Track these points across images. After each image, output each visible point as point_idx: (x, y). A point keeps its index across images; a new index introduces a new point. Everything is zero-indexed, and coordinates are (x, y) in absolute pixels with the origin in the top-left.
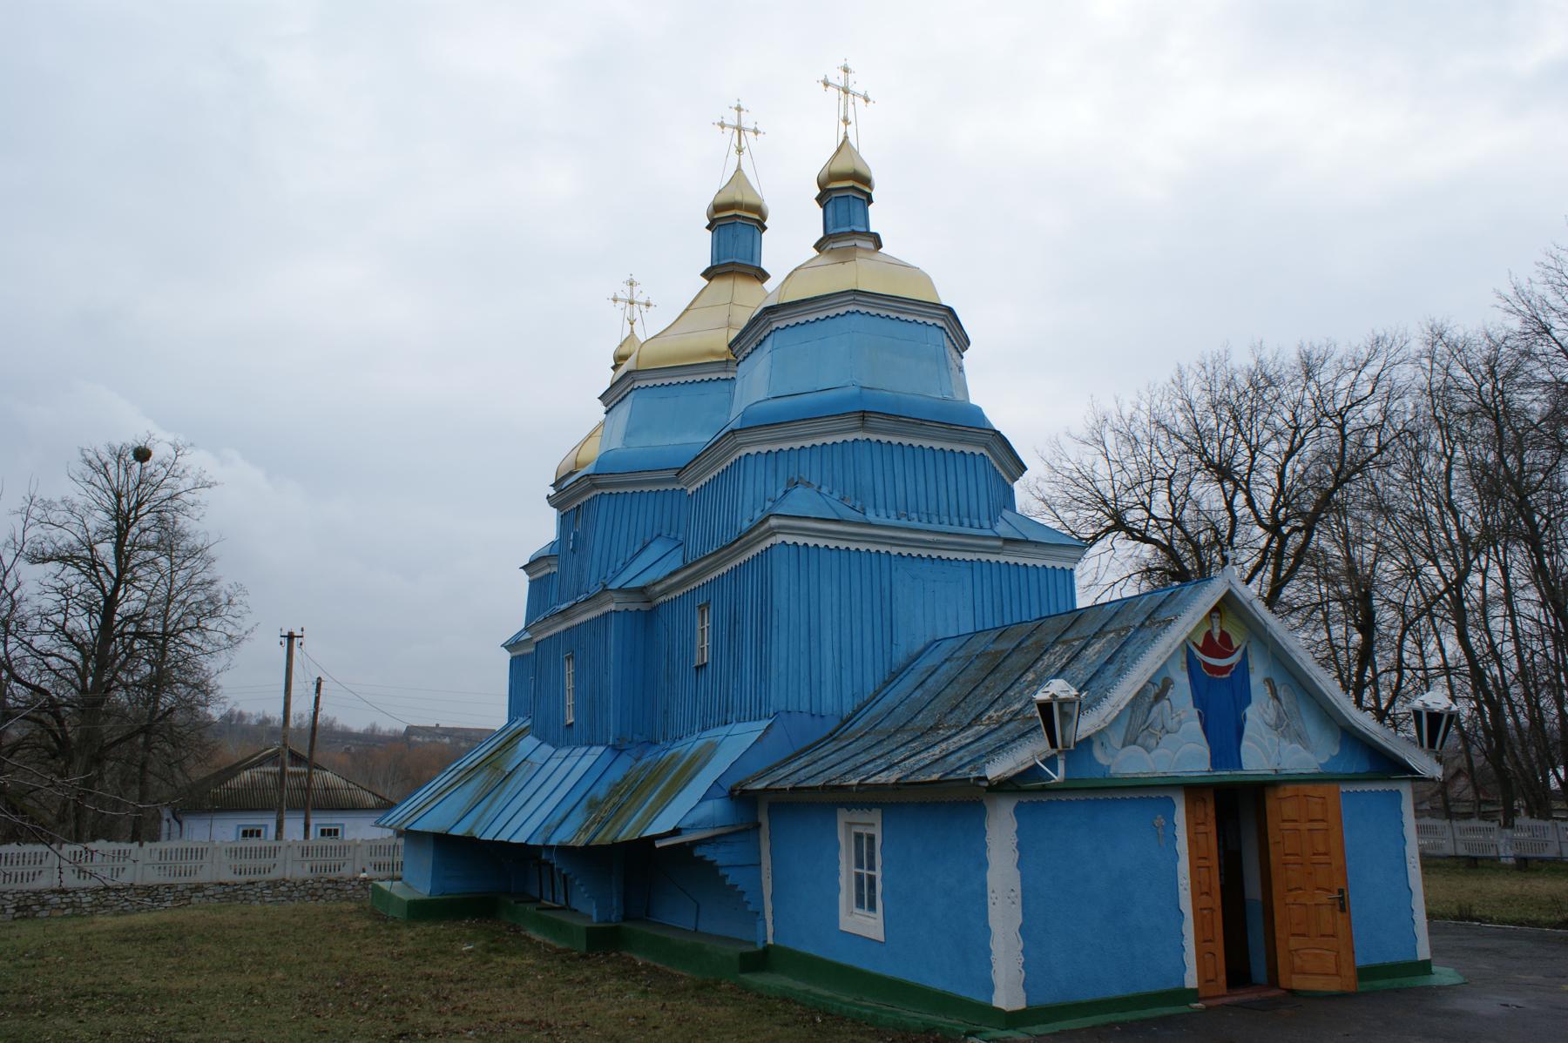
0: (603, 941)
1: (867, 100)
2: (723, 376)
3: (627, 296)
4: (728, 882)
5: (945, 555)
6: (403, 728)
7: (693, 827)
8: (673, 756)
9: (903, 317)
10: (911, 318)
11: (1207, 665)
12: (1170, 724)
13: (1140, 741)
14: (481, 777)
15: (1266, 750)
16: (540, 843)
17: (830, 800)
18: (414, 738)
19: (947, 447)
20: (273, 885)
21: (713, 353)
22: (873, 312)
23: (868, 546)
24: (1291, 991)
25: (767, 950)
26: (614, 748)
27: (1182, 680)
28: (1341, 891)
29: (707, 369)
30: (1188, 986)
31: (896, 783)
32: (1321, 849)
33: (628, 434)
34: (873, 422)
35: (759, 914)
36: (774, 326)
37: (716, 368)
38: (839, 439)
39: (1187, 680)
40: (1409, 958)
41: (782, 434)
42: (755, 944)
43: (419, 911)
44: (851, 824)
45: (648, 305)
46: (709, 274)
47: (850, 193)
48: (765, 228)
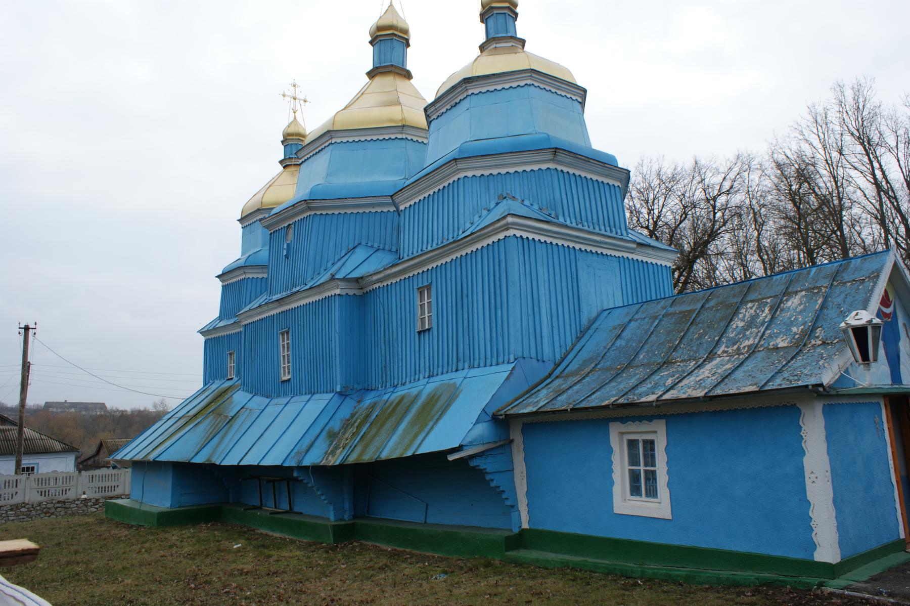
0: (345, 535)
2: (400, 136)
3: (292, 94)
4: (493, 484)
5: (605, 252)
6: (43, 403)
7: (471, 444)
8: (403, 398)
9: (559, 92)
10: (563, 94)
14: (207, 421)
16: (293, 464)
17: (592, 420)
18: (51, 409)
19: (600, 179)
20: (16, 507)
21: (391, 120)
25: (523, 532)
26: (340, 394)
29: (382, 131)
31: (705, 397)
33: (329, 174)
34: (561, 156)
35: (514, 507)
36: (470, 92)
37: (394, 130)
38: (536, 167)
42: (511, 530)
43: (167, 520)
44: (622, 433)
45: (305, 101)
46: (371, 74)
47: (506, 11)
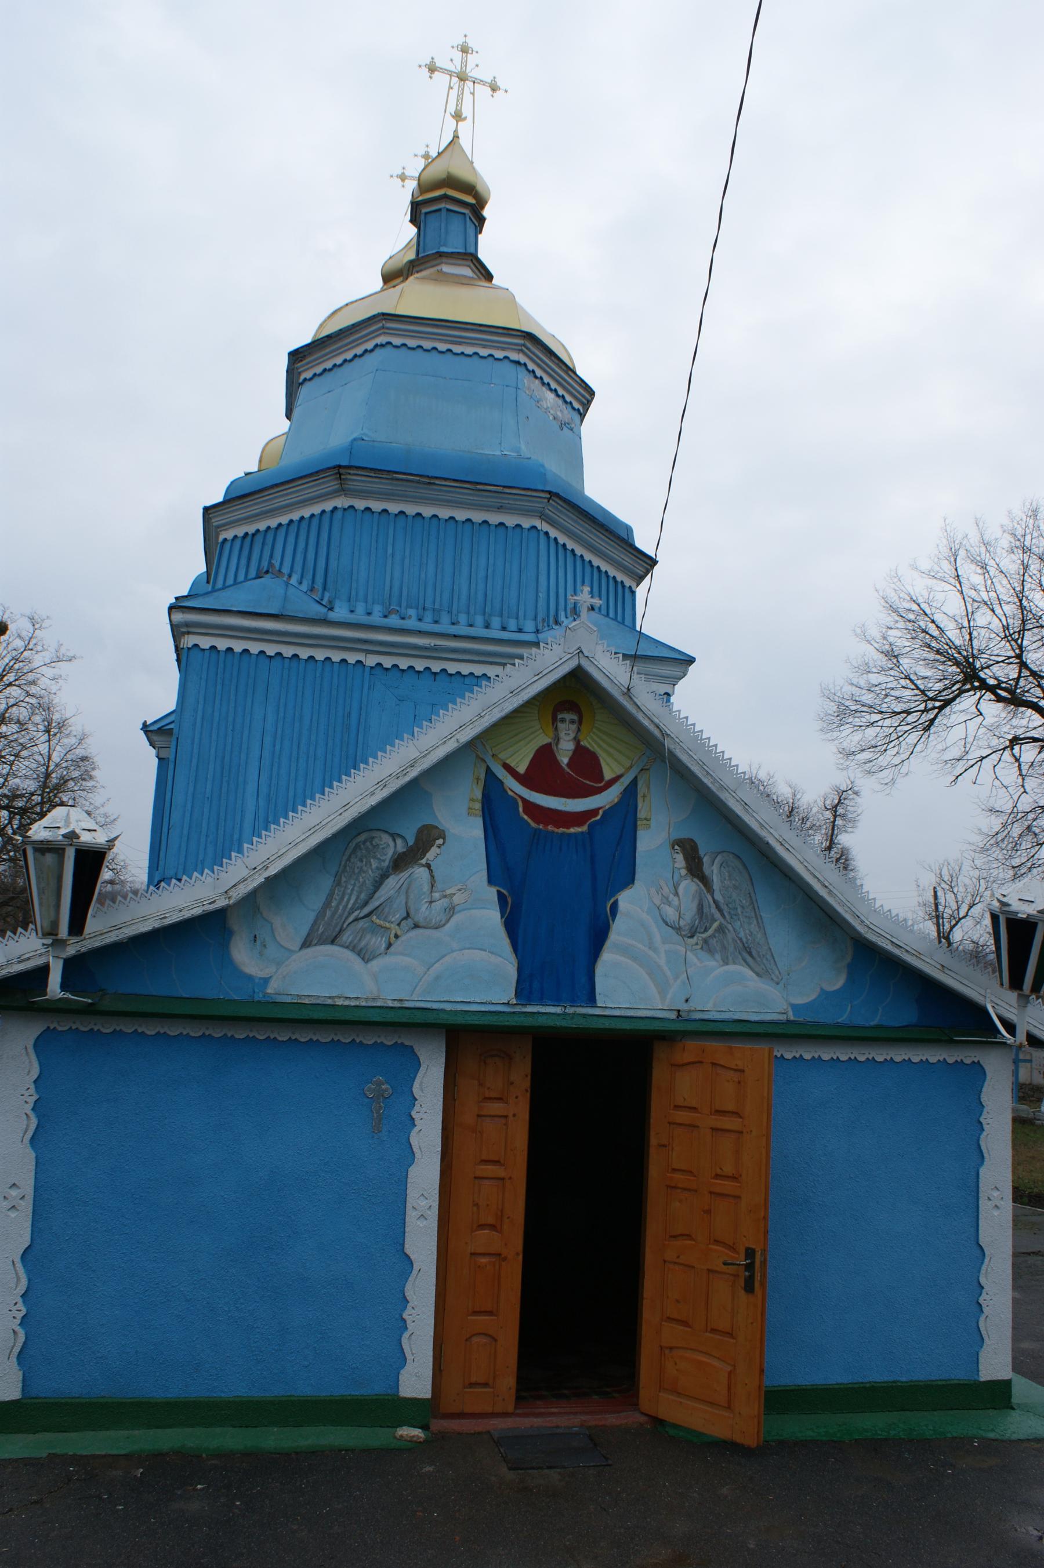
1: (494, 88)
5: (452, 668)
9: (457, 349)
10: (469, 350)
11: (530, 807)
12: (422, 912)
13: (347, 937)
15: (651, 965)
22: (412, 343)
23: (361, 657)
24: (658, 1422)
27: (465, 832)
28: (750, 1253)
32: (728, 1169)
38: (316, 509)
40: (959, 1375)
41: (256, 509)
47: (442, 205)
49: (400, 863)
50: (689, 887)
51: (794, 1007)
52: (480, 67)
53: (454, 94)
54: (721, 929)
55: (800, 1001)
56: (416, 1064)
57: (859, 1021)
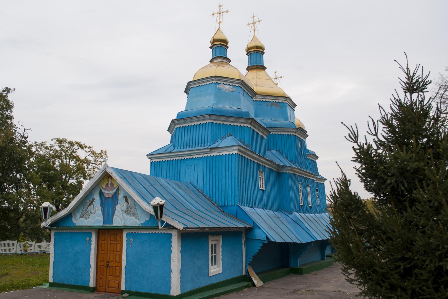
5: (194, 157)
9: (203, 84)
10: (205, 84)
12: (93, 212)
23: (178, 158)
30: (90, 286)
39: (99, 199)
40: (167, 294)
48: (264, 53)
49: (90, 204)
50: (126, 204)
51: (141, 224)
52: (216, 10)
53: (218, 18)
54: (130, 211)
55: (142, 222)
56: (92, 235)
57: (151, 226)
